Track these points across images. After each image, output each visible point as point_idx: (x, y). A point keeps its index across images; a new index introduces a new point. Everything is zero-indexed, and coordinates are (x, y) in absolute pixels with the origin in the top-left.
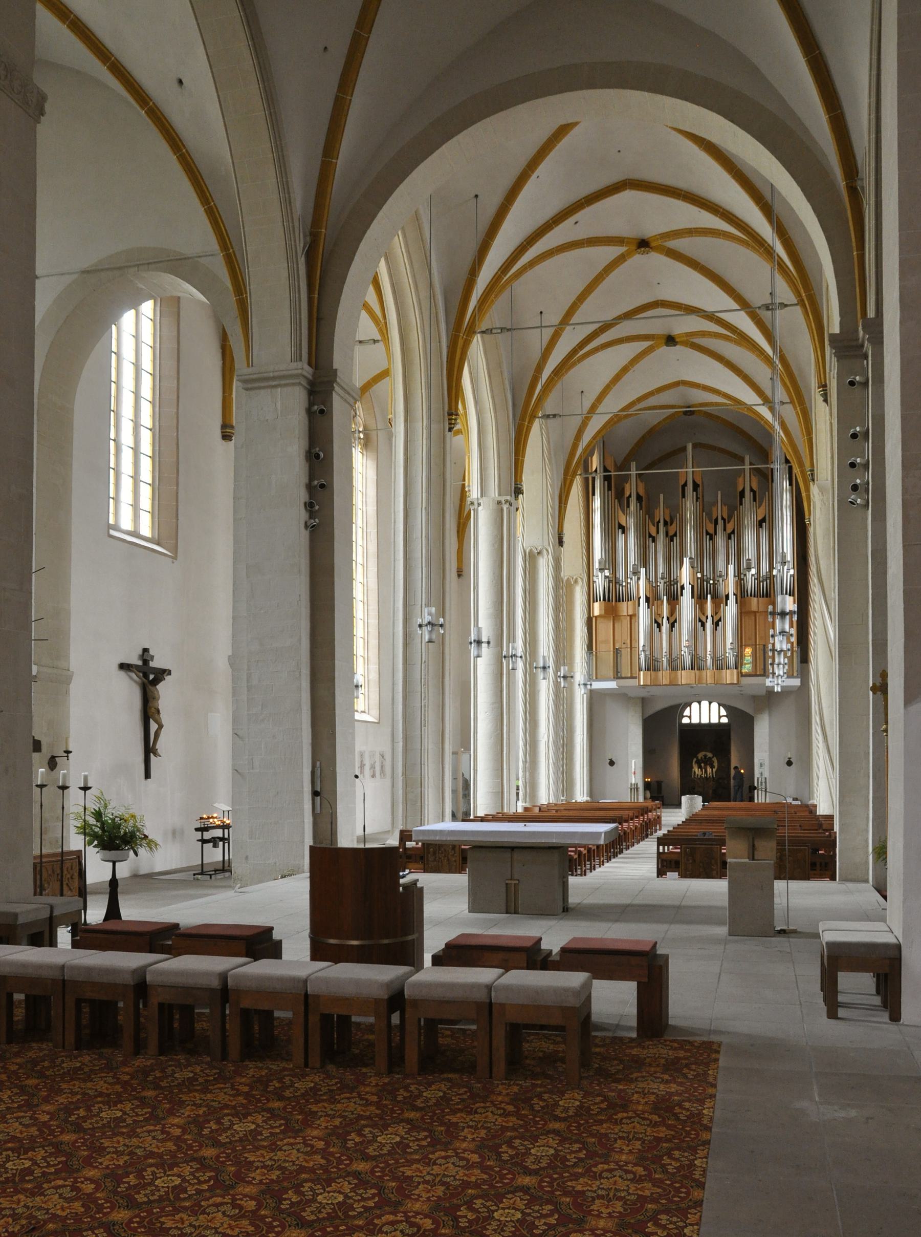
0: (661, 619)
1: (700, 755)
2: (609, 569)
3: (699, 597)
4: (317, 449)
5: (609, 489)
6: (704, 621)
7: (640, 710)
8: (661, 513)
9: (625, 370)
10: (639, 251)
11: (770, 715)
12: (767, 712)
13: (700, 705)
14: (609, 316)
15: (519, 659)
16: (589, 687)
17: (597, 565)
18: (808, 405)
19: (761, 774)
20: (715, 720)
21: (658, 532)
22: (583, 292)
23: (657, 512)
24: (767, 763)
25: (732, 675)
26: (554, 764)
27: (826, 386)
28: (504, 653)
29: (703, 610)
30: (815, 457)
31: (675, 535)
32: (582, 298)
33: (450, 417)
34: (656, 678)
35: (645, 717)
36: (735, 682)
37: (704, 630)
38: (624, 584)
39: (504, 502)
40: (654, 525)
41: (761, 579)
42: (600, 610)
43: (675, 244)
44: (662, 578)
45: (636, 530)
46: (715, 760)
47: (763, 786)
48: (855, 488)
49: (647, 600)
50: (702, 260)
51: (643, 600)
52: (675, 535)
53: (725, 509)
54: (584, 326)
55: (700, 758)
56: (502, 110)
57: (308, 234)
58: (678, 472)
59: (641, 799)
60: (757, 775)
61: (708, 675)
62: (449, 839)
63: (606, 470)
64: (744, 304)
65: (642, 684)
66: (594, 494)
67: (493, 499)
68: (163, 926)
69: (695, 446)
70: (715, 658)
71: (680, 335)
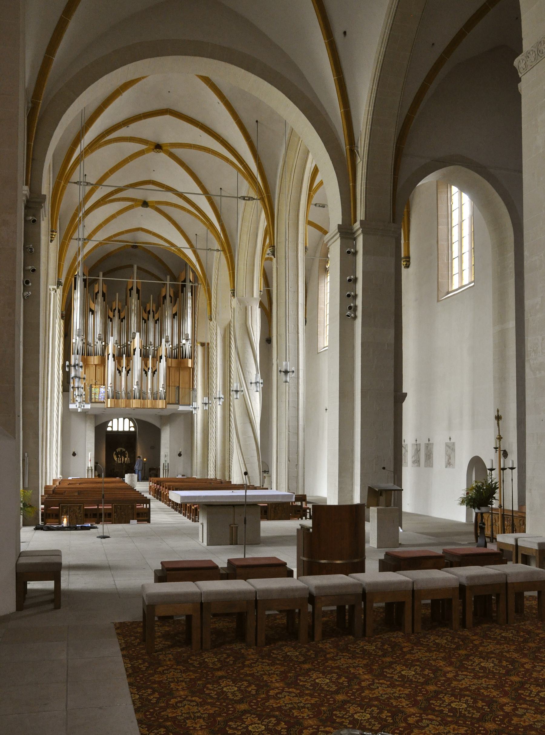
0: (121, 368)
1: (118, 450)
3: (145, 356)
4: (31, 246)
6: (147, 371)
7: (94, 421)
8: (116, 305)
9: (113, 217)
10: (155, 150)
11: (170, 427)
13: (118, 419)
14: (122, 184)
19: (166, 461)
20: (127, 429)
21: (114, 316)
22: (114, 167)
24: (169, 454)
25: (163, 402)
27: (274, 247)
29: (146, 365)
31: (124, 318)
32: (113, 171)
33: (52, 233)
34: (118, 403)
37: (146, 376)
38: (92, 345)
39: (52, 289)
40: (112, 311)
43: (177, 151)
46: (127, 452)
47: (167, 468)
48: (350, 308)
49: (114, 356)
52: (124, 318)
53: (154, 305)
54: (107, 187)
56: (158, 56)
57: (30, 101)
59: (93, 477)
60: (162, 461)
61: (122, 403)
62: (204, 501)
64: (205, 192)
65: (109, 406)
66: (75, 289)
68: (280, 562)
69: (138, 268)
70: (152, 393)
71: (152, 202)
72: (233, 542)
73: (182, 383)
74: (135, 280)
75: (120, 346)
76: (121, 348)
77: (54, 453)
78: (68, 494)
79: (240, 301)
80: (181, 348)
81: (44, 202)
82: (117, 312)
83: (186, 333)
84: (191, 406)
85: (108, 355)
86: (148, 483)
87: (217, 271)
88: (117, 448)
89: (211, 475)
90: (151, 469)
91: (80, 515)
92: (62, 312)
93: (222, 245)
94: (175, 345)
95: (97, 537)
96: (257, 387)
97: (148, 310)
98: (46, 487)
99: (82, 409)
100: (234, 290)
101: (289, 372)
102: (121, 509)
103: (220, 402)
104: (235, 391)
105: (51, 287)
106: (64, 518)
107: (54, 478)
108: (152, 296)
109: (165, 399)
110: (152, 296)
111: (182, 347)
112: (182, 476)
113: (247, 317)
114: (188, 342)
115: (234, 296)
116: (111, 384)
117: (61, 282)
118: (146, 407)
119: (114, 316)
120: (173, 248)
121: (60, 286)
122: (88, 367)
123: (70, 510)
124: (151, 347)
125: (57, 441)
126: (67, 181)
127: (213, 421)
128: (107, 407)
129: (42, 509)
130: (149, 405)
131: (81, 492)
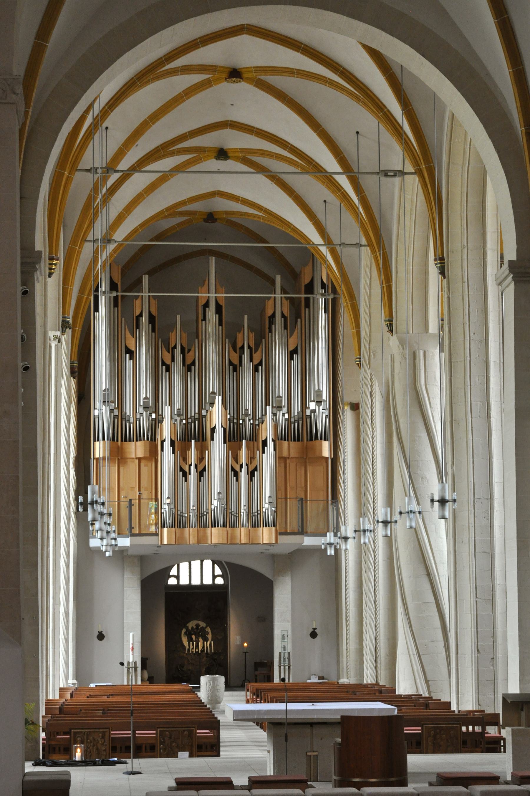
0: (187, 467)
1: (191, 625)
6: (238, 470)
7: (138, 570)
18: (387, 250)
19: (284, 648)
20: (208, 581)
21: (173, 360)
25: (270, 533)
29: (236, 458)
30: (394, 306)
33: (51, 262)
34: (182, 536)
36: (274, 542)
37: (237, 480)
38: (132, 420)
39: (52, 338)
41: (293, 420)
46: (208, 629)
47: (287, 663)
49: (172, 443)
50: (299, 99)
52: (193, 363)
53: (252, 335)
55: (190, 628)
59: (139, 683)
66: (96, 310)
71: (236, 150)
72: (312, 777)
73: (311, 490)
75: (187, 419)
76: (187, 422)
77: (62, 637)
78: (87, 713)
79: (402, 342)
81: (40, 262)
82: (178, 351)
83: (317, 388)
85: (163, 442)
86: (243, 693)
87: (368, 270)
88: (188, 622)
89: (369, 679)
90: (258, 665)
91: (103, 748)
92: (72, 363)
93: (415, 162)
94: (296, 414)
95: (124, 773)
96: (411, 520)
97: (239, 345)
98: (48, 702)
100: (391, 321)
101: (447, 501)
102: (171, 738)
103: (364, 537)
105: (51, 334)
106: (76, 748)
107: (62, 686)
108: (246, 317)
109: (274, 525)
110: (246, 317)
112: (320, 678)
114: (321, 408)
115: (391, 331)
116: (168, 498)
117: (68, 322)
118: (238, 542)
121: (68, 329)
123: (87, 739)
124: (247, 419)
125: (67, 614)
126: (74, 169)
127: (369, 569)
128: (162, 544)
129: (43, 739)
131: (107, 710)
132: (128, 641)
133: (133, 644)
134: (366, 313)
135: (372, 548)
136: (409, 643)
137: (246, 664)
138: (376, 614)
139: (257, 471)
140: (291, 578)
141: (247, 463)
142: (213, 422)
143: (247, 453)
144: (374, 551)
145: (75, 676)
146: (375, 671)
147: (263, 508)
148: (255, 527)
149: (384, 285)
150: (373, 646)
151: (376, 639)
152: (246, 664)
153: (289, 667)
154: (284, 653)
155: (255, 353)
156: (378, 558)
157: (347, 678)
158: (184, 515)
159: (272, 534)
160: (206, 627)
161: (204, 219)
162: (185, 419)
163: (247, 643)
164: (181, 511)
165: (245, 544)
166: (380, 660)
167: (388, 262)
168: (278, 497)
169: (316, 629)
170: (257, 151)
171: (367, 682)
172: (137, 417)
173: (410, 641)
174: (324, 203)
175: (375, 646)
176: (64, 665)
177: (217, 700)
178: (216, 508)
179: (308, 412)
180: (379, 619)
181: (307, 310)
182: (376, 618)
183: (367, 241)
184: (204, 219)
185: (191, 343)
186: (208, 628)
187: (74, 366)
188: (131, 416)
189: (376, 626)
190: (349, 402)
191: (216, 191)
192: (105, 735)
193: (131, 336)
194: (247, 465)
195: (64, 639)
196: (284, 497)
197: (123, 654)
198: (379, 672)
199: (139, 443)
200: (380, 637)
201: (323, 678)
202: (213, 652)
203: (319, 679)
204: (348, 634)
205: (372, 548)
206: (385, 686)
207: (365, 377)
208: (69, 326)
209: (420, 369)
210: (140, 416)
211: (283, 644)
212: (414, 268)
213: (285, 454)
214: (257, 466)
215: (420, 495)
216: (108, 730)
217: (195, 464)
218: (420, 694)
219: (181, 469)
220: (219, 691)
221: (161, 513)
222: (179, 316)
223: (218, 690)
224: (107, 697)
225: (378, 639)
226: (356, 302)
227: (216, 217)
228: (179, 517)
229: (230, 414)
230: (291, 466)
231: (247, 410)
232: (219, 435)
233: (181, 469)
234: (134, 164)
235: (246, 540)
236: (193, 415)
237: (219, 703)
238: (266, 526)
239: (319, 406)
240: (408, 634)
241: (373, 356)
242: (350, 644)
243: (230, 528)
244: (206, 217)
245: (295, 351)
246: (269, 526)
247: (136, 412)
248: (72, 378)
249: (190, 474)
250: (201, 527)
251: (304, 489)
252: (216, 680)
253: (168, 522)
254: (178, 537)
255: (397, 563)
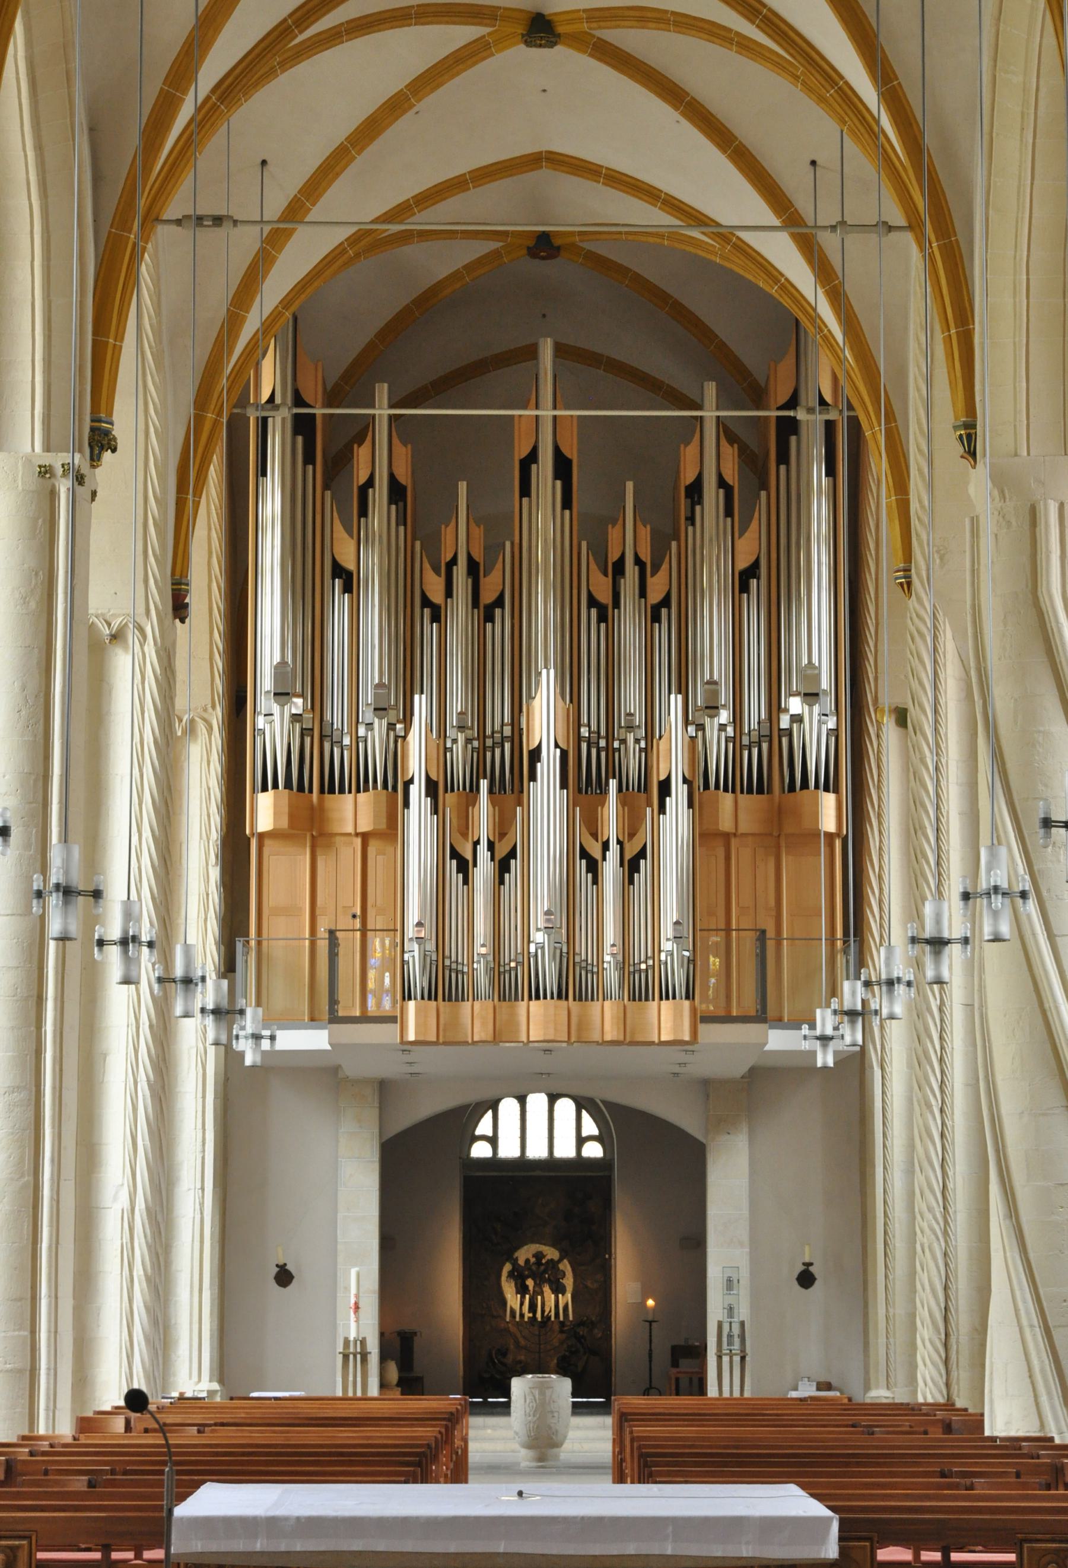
0: (469, 847)
1: (525, 1254)
2: (302, 695)
5: (309, 458)
12: (745, 1128)
15: (145, 950)
16: (265, 1044)
17: (266, 682)
19: (731, 1310)
20: (565, 1149)
21: (449, 593)
23: (448, 534)
24: (744, 1274)
25: (677, 1015)
26: (148, 1279)
28: (1032, 906)
31: (499, 602)
34: (455, 1022)
35: (385, 1138)
36: (687, 1038)
37: (595, 882)
38: (346, 741)
39: (59, 471)
40: (437, 571)
41: (745, 741)
42: (277, 814)
44: (461, 728)
45: (386, 589)
46: (566, 1266)
47: (737, 1346)
49: (432, 788)
51: (417, 791)
52: (499, 602)
53: (645, 533)
55: (521, 1262)
58: (512, 417)
59: (374, 1391)
60: (715, 1312)
63: (299, 401)
67: (28, 460)
69: (561, 351)
70: (625, 964)
71: (573, 16)
74: (547, 413)
79: (1001, 481)
80: (785, 741)
82: (460, 571)
83: (805, 661)
84: (805, 1030)
94: (754, 725)
96: (995, 914)
99: (264, 1053)
104: (928, 942)
108: (630, 486)
110: (630, 486)
111: (789, 733)
113: (1041, 556)
116: (419, 924)
118: (596, 1036)
119: (449, 593)
120: (695, 234)
122: (329, 846)
124: (631, 738)
127: (929, 1106)
130: (608, 1026)
132: (347, 1289)
133: (357, 1296)
134: (920, 450)
135: (936, 1052)
136: (1018, 1293)
137: (651, 1350)
138: (946, 1222)
139: (645, 858)
140: (750, 1141)
141: (621, 839)
142: (533, 734)
143: (620, 812)
144: (941, 1060)
145: (216, 1373)
146: (943, 1372)
147: (660, 951)
148: (640, 999)
149: (953, 331)
150: (938, 1305)
151: (946, 1288)
152: (651, 1350)
153: (743, 1359)
154: (731, 1323)
155: (652, 575)
156: (953, 1078)
157: (888, 1388)
158: (460, 968)
159: (682, 1016)
160: (560, 1260)
161: (529, 248)
162: (478, 739)
163: (654, 1300)
164: (453, 958)
165: (613, 1043)
166: (958, 1342)
167: (964, 269)
168: (698, 927)
169: (811, 1264)
170: (627, 13)
171: (925, 1398)
172: (360, 734)
173: (1021, 1289)
174: (811, 168)
175: (943, 1306)
176: (143, 1343)
177: (552, 1439)
178: (539, 951)
179: (785, 722)
180: (955, 1235)
181: (783, 468)
182: (945, 1233)
183: (908, 218)
184: (529, 248)
185: (493, 549)
186: (566, 1261)
187: (180, 590)
188: (346, 731)
189: (945, 1254)
190: (893, 706)
191: (541, 152)
192: (15, 1557)
193: (346, 536)
194: (619, 842)
195: (143, 1278)
196: (722, 926)
197: (335, 1318)
198: (954, 1374)
199: (362, 797)
200: (956, 1281)
201: (828, 1387)
202: (571, 1318)
203: (818, 1389)
204: (891, 1277)
205: (936, 1052)
206: (966, 1410)
207: (918, 616)
208: (109, 444)
209: (1048, 553)
210: (367, 730)
211: (730, 1299)
212: (1031, 277)
213: (726, 824)
214: (645, 845)
215: (1049, 890)
216: (25, 1542)
217: (489, 840)
218: (1049, 1435)
219: (455, 854)
220: (556, 1414)
221: (403, 961)
222: (465, 483)
223: (552, 1412)
224: (199, 1432)
225: (952, 1287)
226: (896, 426)
227: (557, 242)
228: (447, 973)
229: (589, 726)
230: (742, 855)
231: (630, 714)
232: (549, 767)
233: (455, 854)
234: (285, 20)
235: (615, 1033)
236: (497, 727)
237: (558, 1445)
238: (667, 998)
239: (811, 705)
240: (1016, 1270)
241: (938, 561)
242: (894, 1303)
243: (577, 1002)
244: (531, 243)
245: (750, 573)
246: (674, 998)
247: (358, 722)
248: (177, 620)
249: (475, 865)
250: (502, 998)
251: (774, 913)
252: (548, 1388)
253: (419, 980)
254: (445, 1025)
255: (986, 1076)
